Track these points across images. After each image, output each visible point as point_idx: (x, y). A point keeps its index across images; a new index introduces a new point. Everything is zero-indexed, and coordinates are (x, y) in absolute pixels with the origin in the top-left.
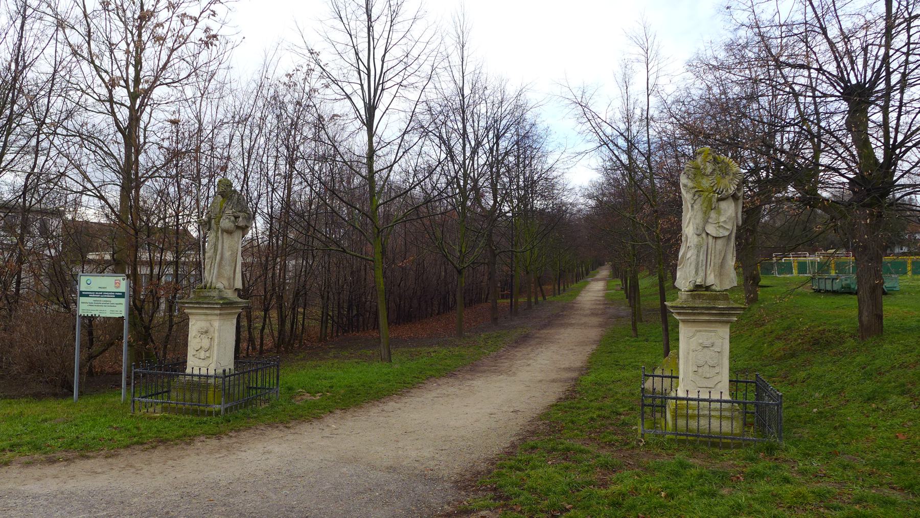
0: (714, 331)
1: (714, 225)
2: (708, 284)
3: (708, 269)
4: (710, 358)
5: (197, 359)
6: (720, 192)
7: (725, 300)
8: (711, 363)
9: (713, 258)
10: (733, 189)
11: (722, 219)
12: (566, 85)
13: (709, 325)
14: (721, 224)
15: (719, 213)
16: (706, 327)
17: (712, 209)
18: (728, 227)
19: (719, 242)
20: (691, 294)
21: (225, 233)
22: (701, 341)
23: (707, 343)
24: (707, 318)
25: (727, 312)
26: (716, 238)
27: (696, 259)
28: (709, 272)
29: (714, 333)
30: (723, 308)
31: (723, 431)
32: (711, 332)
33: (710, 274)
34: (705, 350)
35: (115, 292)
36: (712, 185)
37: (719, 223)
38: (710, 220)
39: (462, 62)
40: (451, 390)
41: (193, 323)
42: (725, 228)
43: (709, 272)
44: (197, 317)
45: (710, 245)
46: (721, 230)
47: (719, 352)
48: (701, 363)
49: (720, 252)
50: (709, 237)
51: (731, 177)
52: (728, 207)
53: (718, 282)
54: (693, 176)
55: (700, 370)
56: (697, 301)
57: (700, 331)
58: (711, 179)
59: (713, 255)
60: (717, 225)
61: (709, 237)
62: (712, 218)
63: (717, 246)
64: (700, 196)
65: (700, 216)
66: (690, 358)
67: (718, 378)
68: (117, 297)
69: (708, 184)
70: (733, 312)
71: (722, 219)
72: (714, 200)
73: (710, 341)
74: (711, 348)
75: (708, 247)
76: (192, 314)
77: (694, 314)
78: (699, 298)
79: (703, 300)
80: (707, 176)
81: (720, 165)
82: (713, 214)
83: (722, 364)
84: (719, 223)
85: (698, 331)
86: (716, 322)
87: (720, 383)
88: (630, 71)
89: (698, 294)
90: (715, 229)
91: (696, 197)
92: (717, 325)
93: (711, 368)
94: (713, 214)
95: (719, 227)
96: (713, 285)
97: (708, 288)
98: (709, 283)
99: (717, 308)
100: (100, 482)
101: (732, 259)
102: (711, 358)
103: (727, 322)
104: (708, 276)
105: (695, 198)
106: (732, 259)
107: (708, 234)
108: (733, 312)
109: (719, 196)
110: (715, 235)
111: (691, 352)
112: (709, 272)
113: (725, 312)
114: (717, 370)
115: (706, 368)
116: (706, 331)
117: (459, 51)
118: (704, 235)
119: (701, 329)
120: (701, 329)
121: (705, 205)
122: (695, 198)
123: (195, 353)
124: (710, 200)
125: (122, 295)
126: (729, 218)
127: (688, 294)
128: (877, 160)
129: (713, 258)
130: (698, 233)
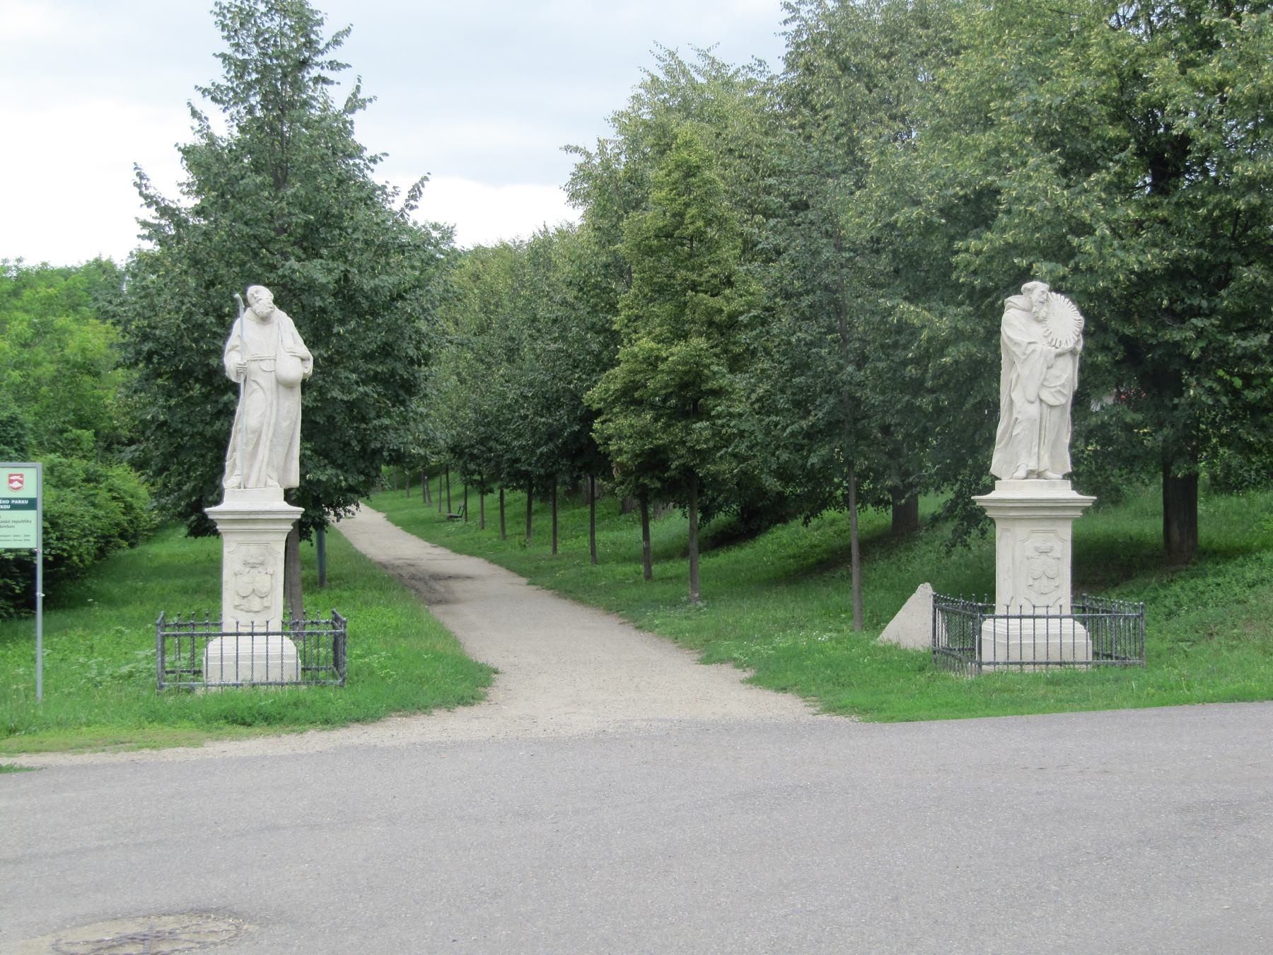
2: (1041, 470)
5: (243, 613)
6: (1057, 345)
8: (1051, 574)
21: (281, 388)
23: (1044, 547)
26: (1051, 407)
35: (10, 499)
41: (231, 549)
44: (240, 538)
45: (1044, 416)
47: (1058, 559)
50: (1044, 405)
55: (1036, 584)
68: (15, 507)
76: (232, 532)
85: (1033, 532)
88: (931, 275)
100: (364, 739)
103: (1065, 518)
114: (1057, 582)
116: (1045, 532)
123: (238, 601)
125: (31, 504)
128: (974, 495)
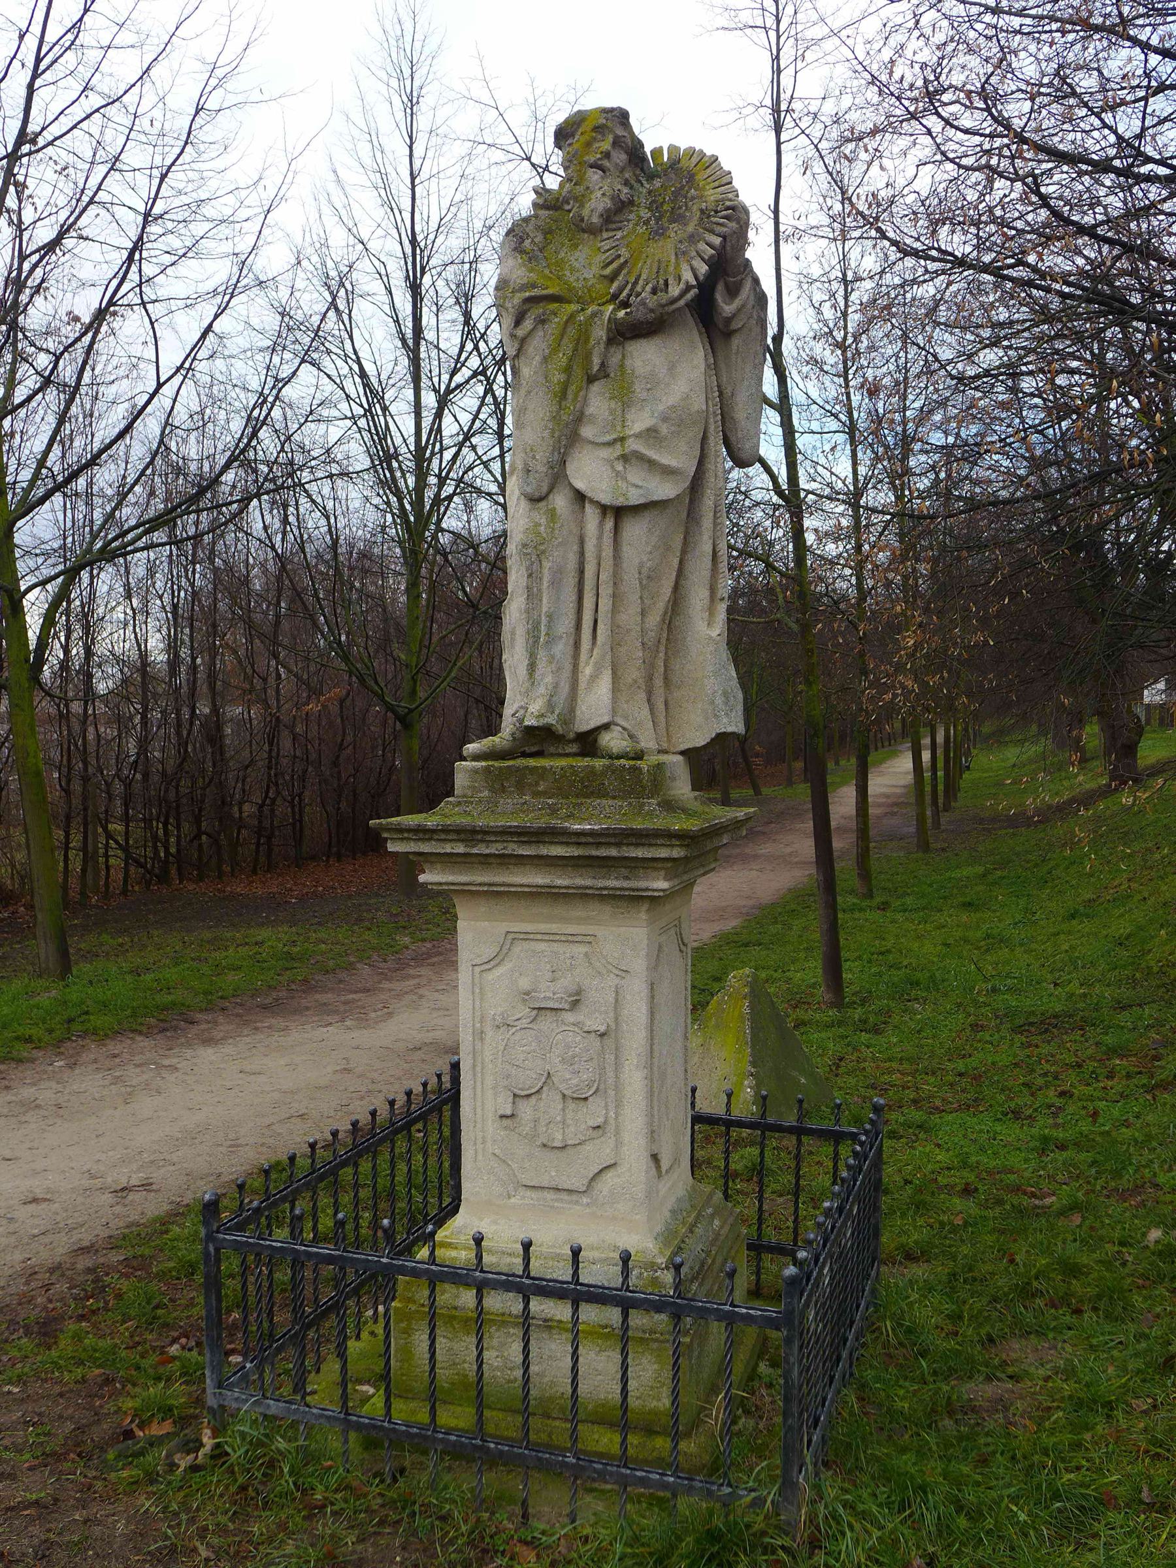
0: (587, 940)
1: (605, 453)
3: (583, 656)
4: (563, 1061)
7: (625, 794)
8: (566, 1079)
9: (605, 604)
10: (688, 276)
11: (639, 421)
12: (486, 97)
13: (560, 910)
14: (633, 445)
15: (624, 397)
16: (550, 919)
17: (591, 380)
18: (673, 463)
19: (636, 531)
20: (487, 770)
22: (524, 983)
23: (552, 992)
24: (539, 878)
25: (613, 852)
26: (618, 513)
27: (527, 611)
28: (587, 671)
29: (582, 949)
30: (592, 833)
31: (633, 1402)
32: (571, 939)
33: (594, 678)
34: (546, 1023)
36: (608, 271)
37: (622, 439)
38: (587, 431)
39: (411, 147)
40: (46, 1093)
42: (651, 463)
43: (588, 671)
46: (636, 475)
48: (528, 1079)
49: (649, 579)
51: (690, 228)
52: (672, 367)
53: (638, 712)
54: (539, 239)
55: (526, 1110)
56: (508, 803)
57: (527, 937)
58: (606, 245)
59: (606, 591)
60: (618, 450)
61: (589, 508)
62: (592, 419)
63: (627, 551)
64: (541, 321)
65: (540, 408)
66: (488, 1055)
67: (599, 1152)
69: (595, 270)
70: (639, 853)
71: (639, 421)
72: (599, 333)
73: (566, 983)
74: (570, 1017)
75: (582, 553)
76: (471, 893)
77: (485, 861)
78: (520, 787)
79: (536, 794)
80: (593, 231)
81: (657, 183)
82: (598, 403)
83: (617, 1088)
84: (622, 439)
85: (514, 938)
86: (583, 896)
87: (610, 1174)
89: (518, 769)
90: (607, 472)
91: (528, 324)
92: (595, 910)
93: (571, 1105)
94: (598, 403)
95: (625, 458)
96: (606, 727)
97: (588, 742)
98: (588, 717)
99: (565, 832)
101: (711, 611)
102: (568, 1061)
104: (582, 685)
105: (520, 332)
106: (711, 611)
107: (580, 497)
108: (639, 853)
109: (621, 314)
110: (606, 499)
111: (490, 1034)
112: (588, 671)
113: (603, 852)
114: (594, 1113)
115: (551, 1103)
116: (550, 938)
117: (400, 115)
118: (561, 501)
119: (529, 927)
120: (529, 927)
121: (562, 359)
122: (520, 332)
124: (583, 337)
126: (676, 418)
127: (475, 771)
129: (605, 604)
130: (529, 490)
